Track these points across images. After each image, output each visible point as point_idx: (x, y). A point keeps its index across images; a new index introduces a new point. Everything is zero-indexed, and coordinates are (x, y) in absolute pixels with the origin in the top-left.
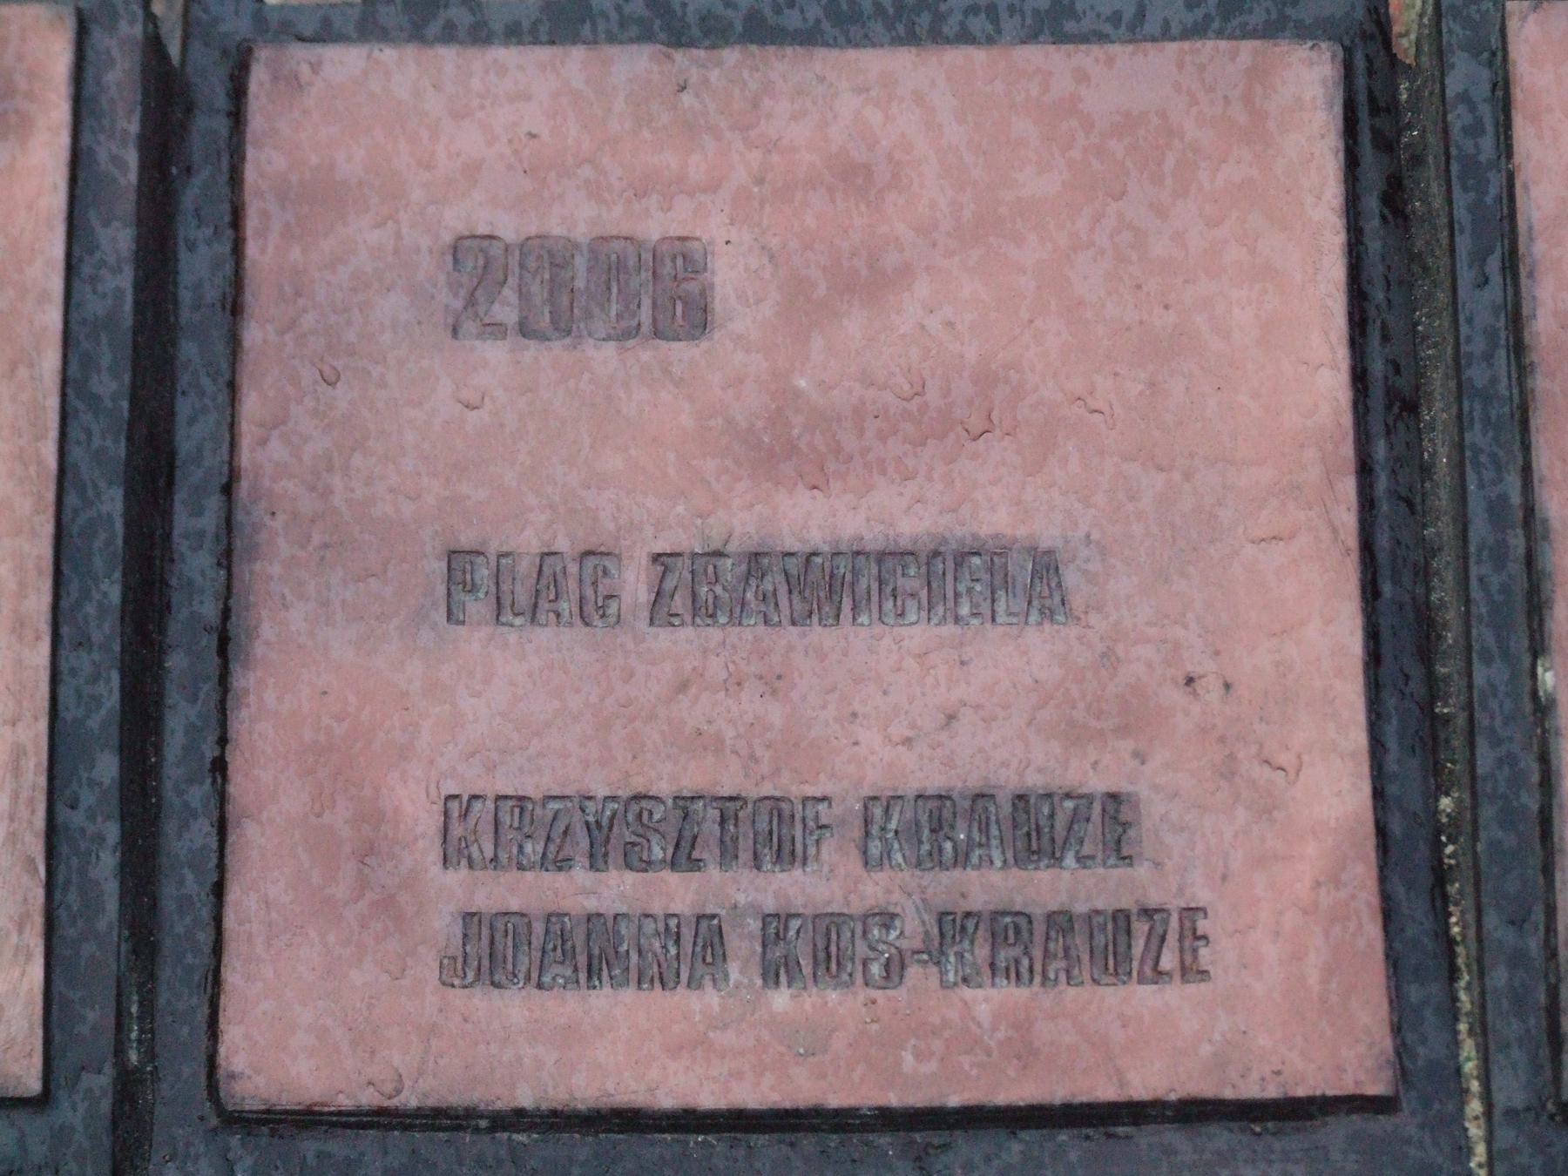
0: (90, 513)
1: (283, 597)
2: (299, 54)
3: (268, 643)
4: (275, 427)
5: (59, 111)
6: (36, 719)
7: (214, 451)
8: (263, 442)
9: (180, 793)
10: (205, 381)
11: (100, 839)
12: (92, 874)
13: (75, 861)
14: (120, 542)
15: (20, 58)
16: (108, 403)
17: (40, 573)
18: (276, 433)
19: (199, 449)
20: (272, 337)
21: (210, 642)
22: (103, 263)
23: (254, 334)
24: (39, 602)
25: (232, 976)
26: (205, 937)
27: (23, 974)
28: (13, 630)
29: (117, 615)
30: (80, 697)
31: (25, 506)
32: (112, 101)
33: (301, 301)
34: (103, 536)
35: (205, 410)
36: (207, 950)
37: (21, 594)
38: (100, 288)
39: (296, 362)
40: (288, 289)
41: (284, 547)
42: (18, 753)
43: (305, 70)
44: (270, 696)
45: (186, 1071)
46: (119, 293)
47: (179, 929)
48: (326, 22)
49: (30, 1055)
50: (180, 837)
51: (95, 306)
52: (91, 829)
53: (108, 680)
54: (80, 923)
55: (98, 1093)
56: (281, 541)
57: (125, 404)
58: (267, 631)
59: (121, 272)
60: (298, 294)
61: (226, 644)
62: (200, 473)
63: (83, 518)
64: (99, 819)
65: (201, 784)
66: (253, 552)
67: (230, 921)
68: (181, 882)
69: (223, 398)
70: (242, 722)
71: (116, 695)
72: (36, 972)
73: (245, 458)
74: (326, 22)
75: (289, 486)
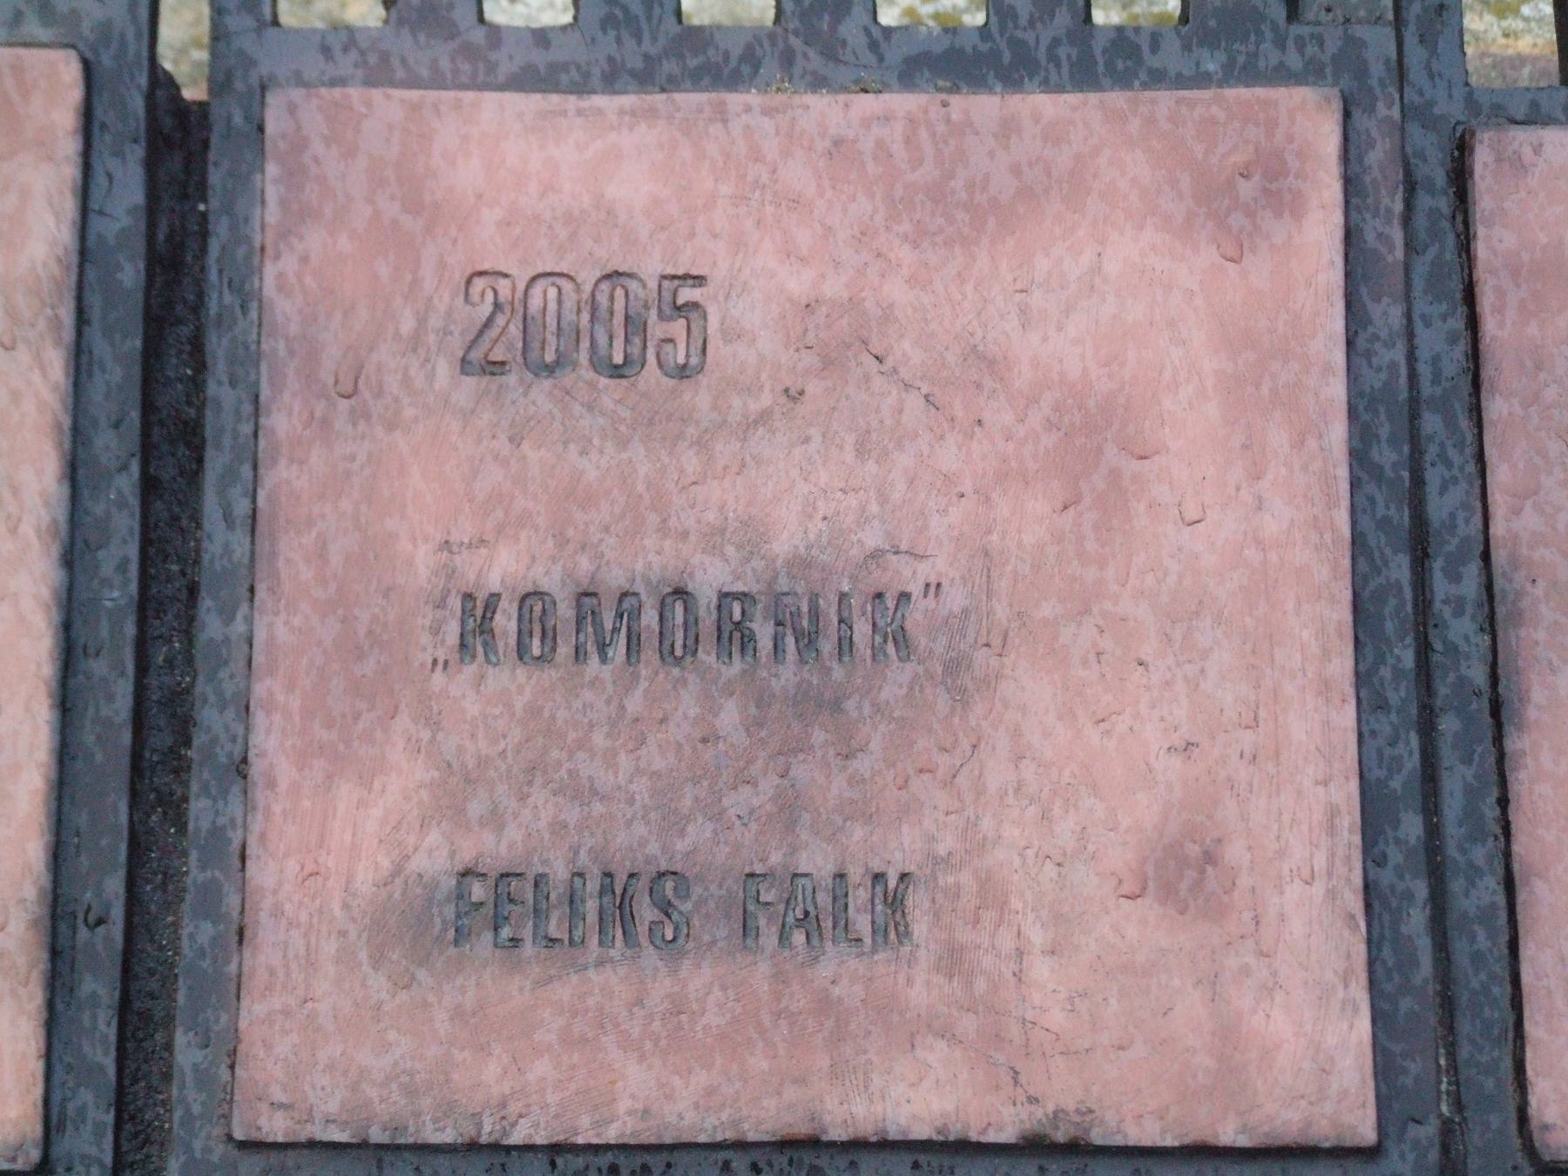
0: (1381, 580)
1: (1550, 663)
2: (1521, 137)
3: (1539, 708)
4: (1526, 498)
5: (1331, 189)
6: (1347, 778)
7: (1467, 522)
8: (1517, 512)
9: (1463, 851)
10: (1452, 453)
11: (1409, 896)
12: (1404, 929)
13: (1386, 917)
14: (1409, 608)
15: (1290, 139)
16: (1389, 473)
17: (1340, 635)
18: (1529, 503)
19: (1452, 516)
20: (1518, 410)
21: (1482, 706)
22: (1376, 337)
23: (1496, 408)
24: (1342, 666)
25: (1534, 1029)
26: (1502, 992)
27: (1351, 1027)
28: (1320, 694)
29: (1412, 676)
30: (1381, 760)
31: (1322, 573)
32: (1374, 181)
33: (1542, 376)
34: (1393, 602)
35: (1455, 481)
36: (1505, 1003)
37: (1326, 654)
38: (1375, 360)
39: (1543, 434)
40: (1529, 364)
41: (1547, 613)
42: (1333, 813)
43: (1527, 151)
44: (1546, 759)
45: (1495, 1121)
46: (1393, 365)
47: (1475, 984)
48: (1534, 105)
49: (1364, 1105)
50: (1467, 895)
51: (1373, 380)
52: (1401, 887)
53: (1408, 743)
54: (1397, 978)
55: (1424, 1142)
56: (1543, 609)
57: (1406, 474)
58: (1538, 695)
59: (1394, 345)
60: (1539, 367)
61: (1498, 711)
62: (1455, 541)
63: (1372, 585)
64: (1407, 877)
65: (1484, 842)
66: (1517, 618)
67: (1526, 977)
68: (1473, 939)
69: (1471, 468)
70: (1522, 782)
71: (1417, 756)
72: (1363, 1025)
73: (1498, 529)
74: (1534, 105)
75: (1543, 554)
